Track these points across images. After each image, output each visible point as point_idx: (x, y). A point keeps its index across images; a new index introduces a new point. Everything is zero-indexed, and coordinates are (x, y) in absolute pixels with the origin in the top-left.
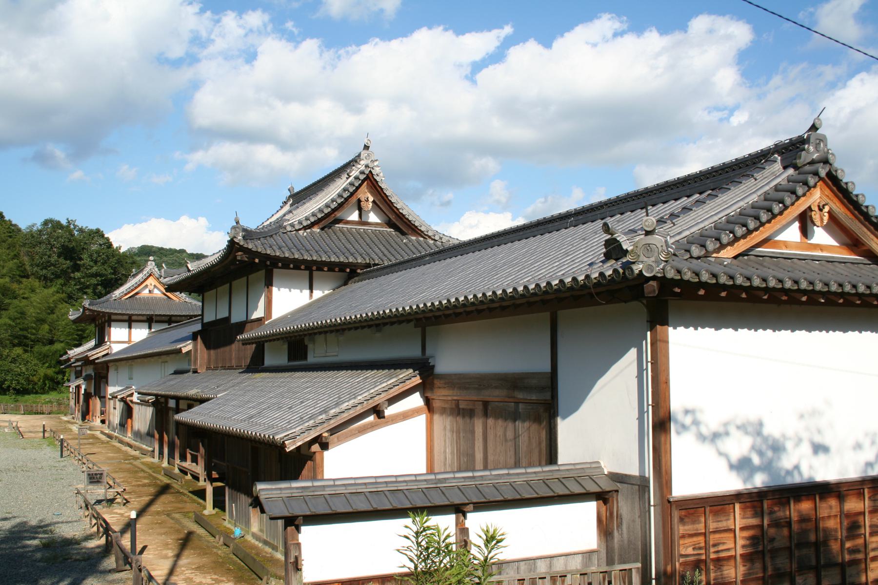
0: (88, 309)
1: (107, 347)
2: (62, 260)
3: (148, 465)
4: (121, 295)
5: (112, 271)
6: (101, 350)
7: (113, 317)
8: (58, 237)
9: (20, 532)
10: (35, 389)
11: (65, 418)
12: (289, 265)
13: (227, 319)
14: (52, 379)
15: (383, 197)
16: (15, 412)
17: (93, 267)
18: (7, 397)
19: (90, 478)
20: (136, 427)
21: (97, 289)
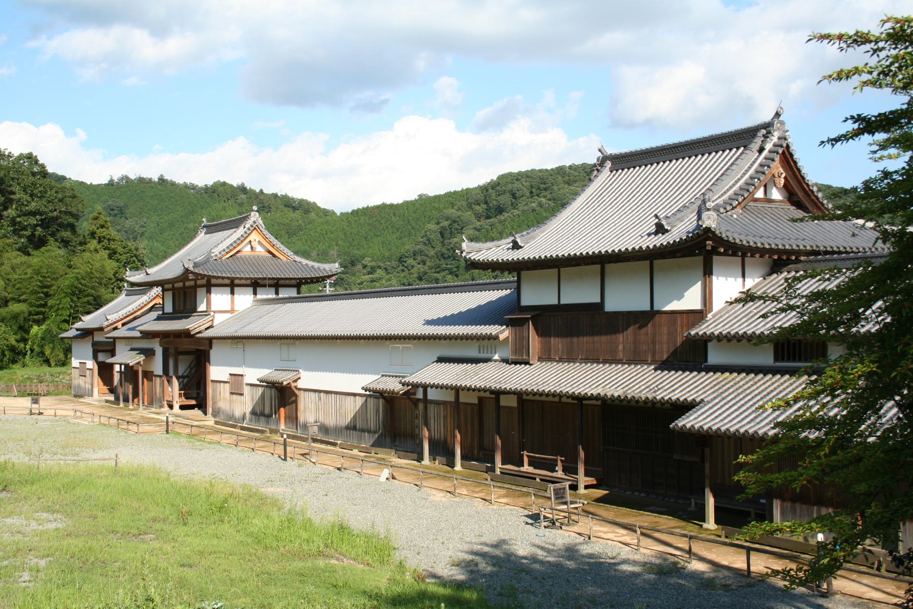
0: (192, 272)
14: (13, 349)
15: (794, 173)
16: (6, 394)
21: (35, 230)
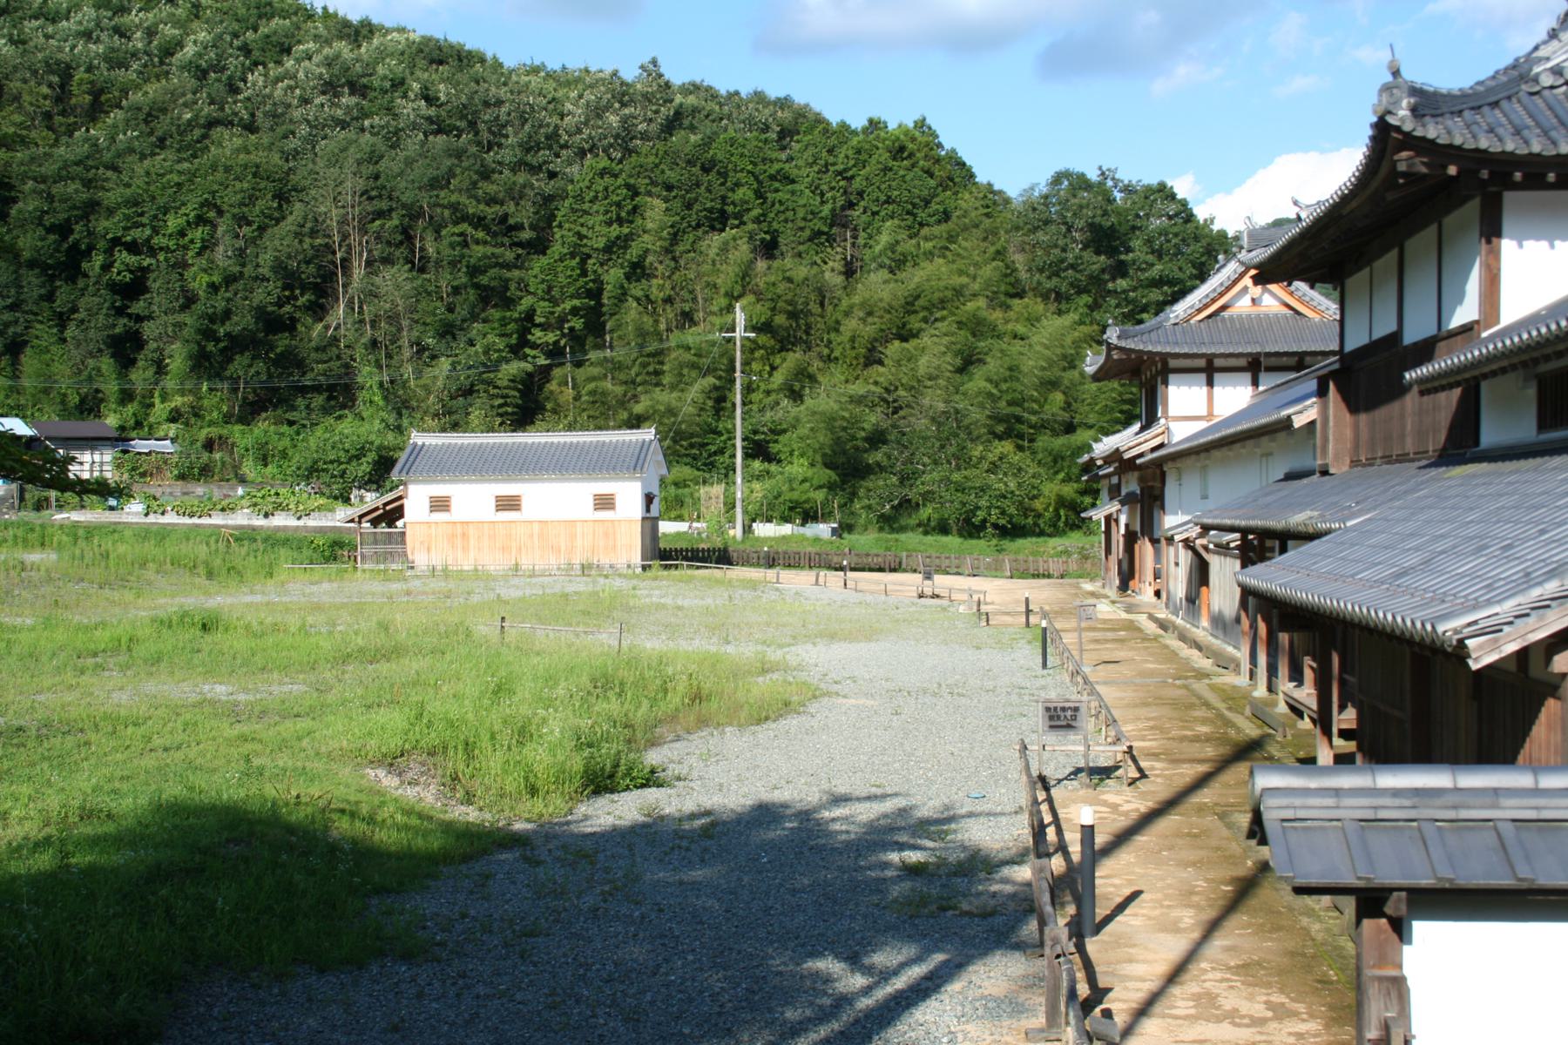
1: (1160, 430)
2: (1088, 255)
3: (1224, 690)
4: (1189, 312)
5: (1194, 272)
6: (1148, 437)
7: (1173, 363)
8: (1081, 207)
9: (892, 829)
10: (1039, 526)
11: (1088, 586)
12: (1544, 175)
13: (1395, 337)
16: (994, 573)
17: (1153, 265)
18: (982, 542)
19: (1051, 718)
20: (1215, 608)
